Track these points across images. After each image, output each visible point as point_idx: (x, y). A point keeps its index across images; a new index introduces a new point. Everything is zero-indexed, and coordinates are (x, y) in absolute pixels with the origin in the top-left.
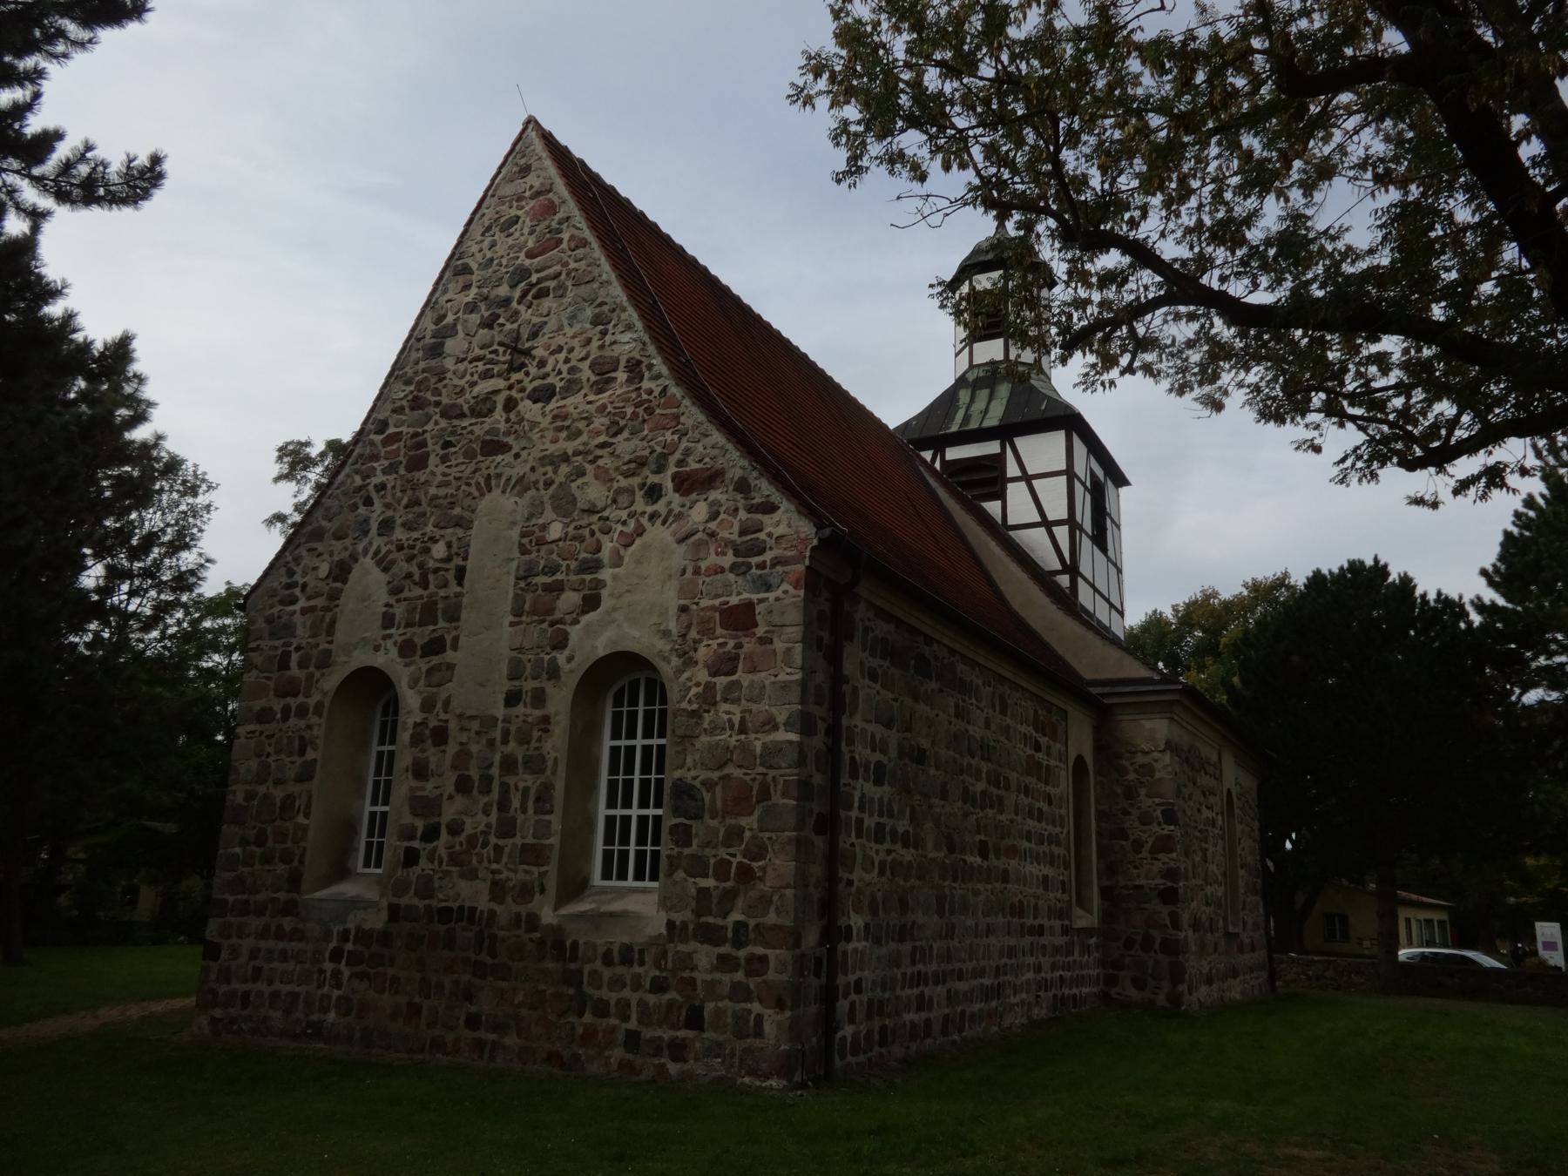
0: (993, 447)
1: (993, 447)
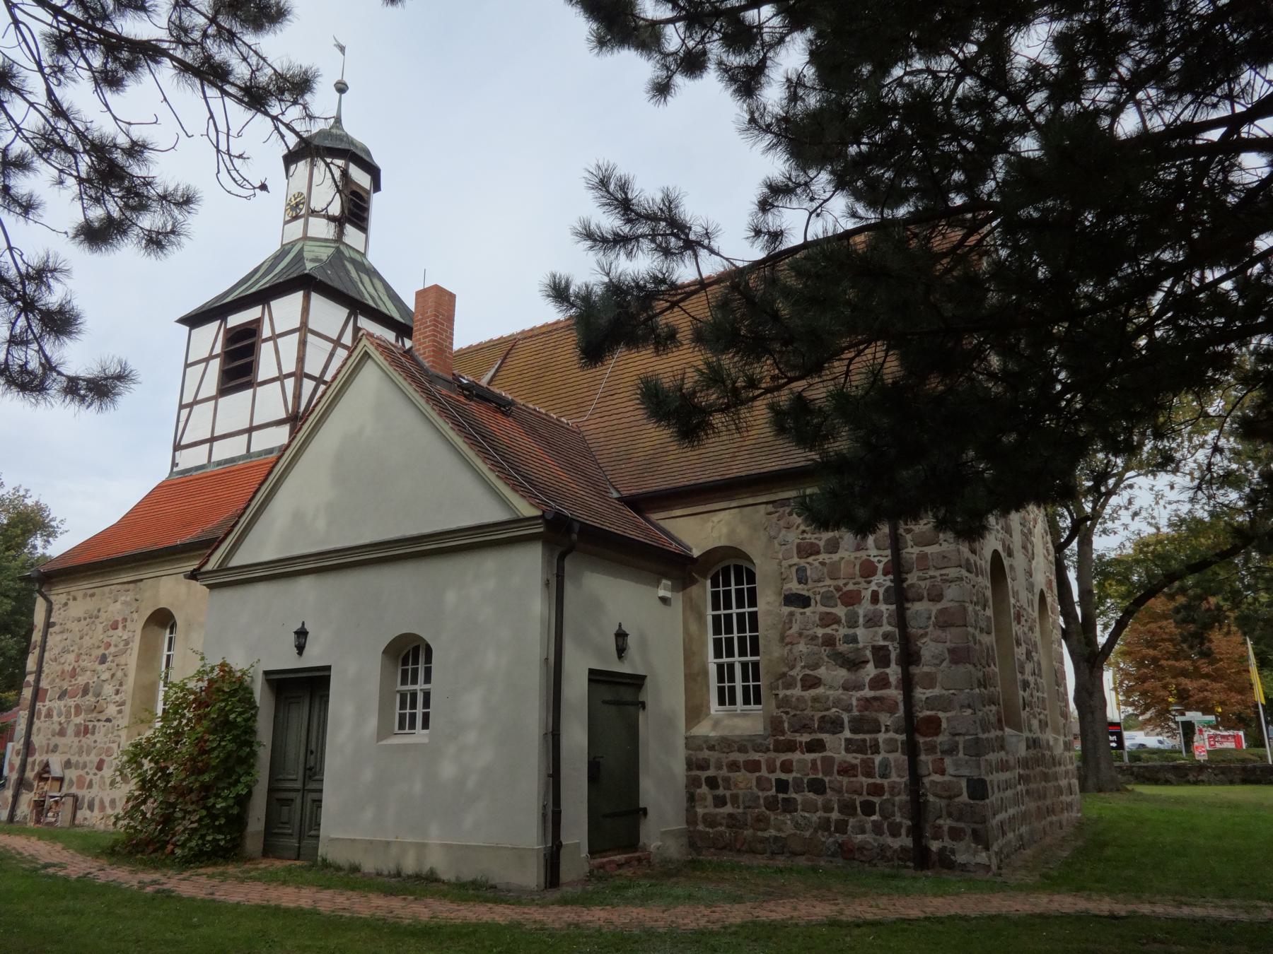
0: (253, 313)
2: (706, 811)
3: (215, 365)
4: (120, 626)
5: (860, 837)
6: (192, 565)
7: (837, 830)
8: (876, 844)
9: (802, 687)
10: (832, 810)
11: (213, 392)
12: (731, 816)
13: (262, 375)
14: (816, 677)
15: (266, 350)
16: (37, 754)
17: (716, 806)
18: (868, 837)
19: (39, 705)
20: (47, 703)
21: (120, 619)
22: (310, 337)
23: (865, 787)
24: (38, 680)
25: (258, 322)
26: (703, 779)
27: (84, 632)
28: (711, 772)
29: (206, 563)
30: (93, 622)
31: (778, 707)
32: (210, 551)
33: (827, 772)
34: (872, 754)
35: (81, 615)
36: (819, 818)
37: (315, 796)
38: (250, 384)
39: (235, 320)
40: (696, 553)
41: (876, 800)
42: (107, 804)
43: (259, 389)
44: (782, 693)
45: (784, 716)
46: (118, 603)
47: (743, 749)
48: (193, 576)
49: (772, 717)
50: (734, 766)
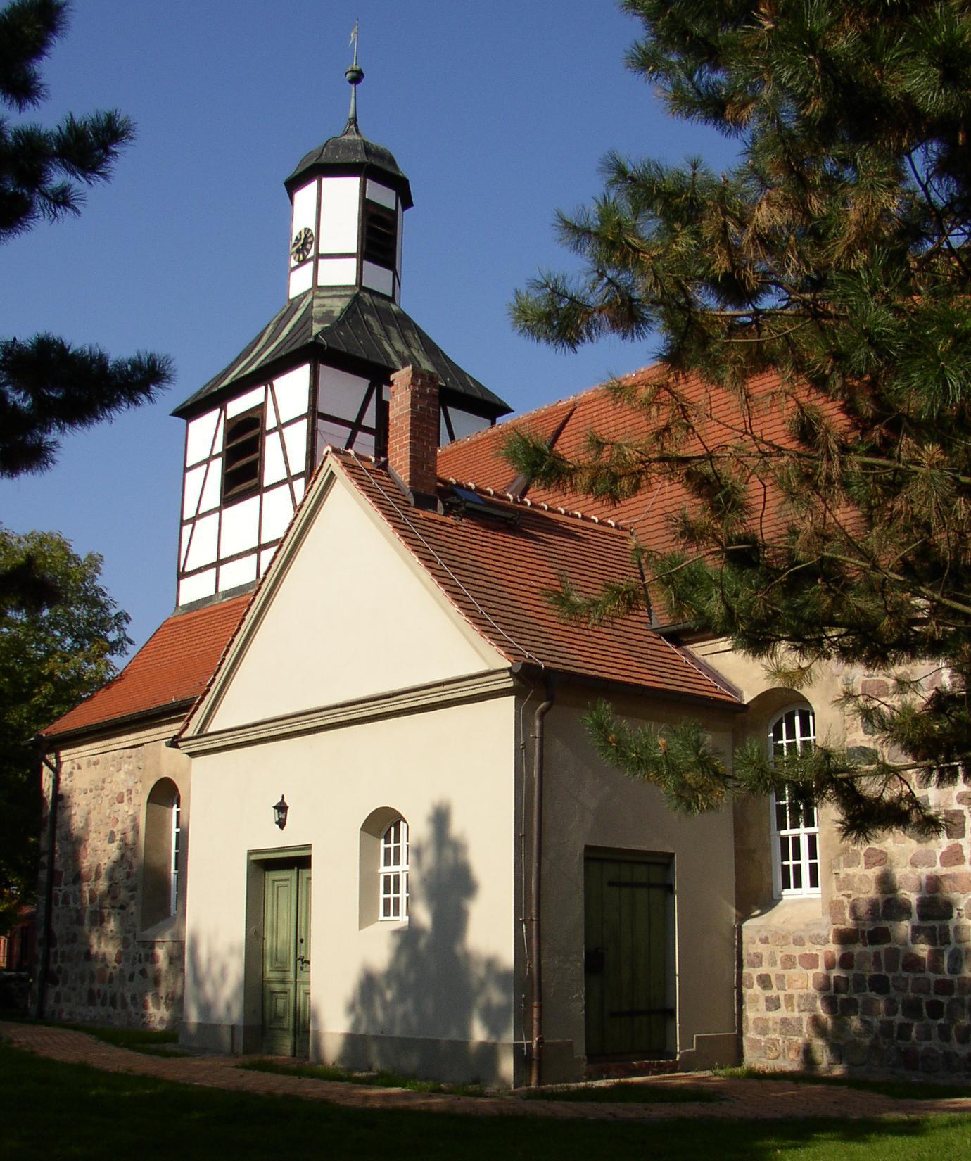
0: (252, 399)
2: (758, 1015)
3: (217, 465)
4: (126, 798)
5: (925, 1044)
6: (171, 730)
7: (899, 1037)
8: (941, 1052)
9: (866, 864)
10: (895, 1012)
11: (217, 503)
12: (784, 1021)
13: (270, 477)
14: (881, 852)
15: (271, 442)
16: (58, 946)
17: (768, 1009)
18: (935, 1043)
19: (56, 889)
20: (63, 887)
21: (124, 791)
22: (321, 424)
23: (932, 984)
24: (52, 861)
25: (262, 407)
26: (755, 977)
27: (92, 806)
28: (763, 970)
29: (186, 728)
30: (99, 795)
31: (839, 889)
32: (189, 714)
33: (892, 967)
34: (942, 944)
35: (87, 786)
36: (881, 1022)
37: (305, 987)
38: (259, 490)
39: (238, 407)
40: (747, 698)
41: (943, 999)
42: (129, 1000)
43: (265, 495)
44: (844, 871)
45: (846, 900)
46: (122, 772)
47: (799, 941)
48: (174, 743)
49: (832, 902)
50: (789, 962)
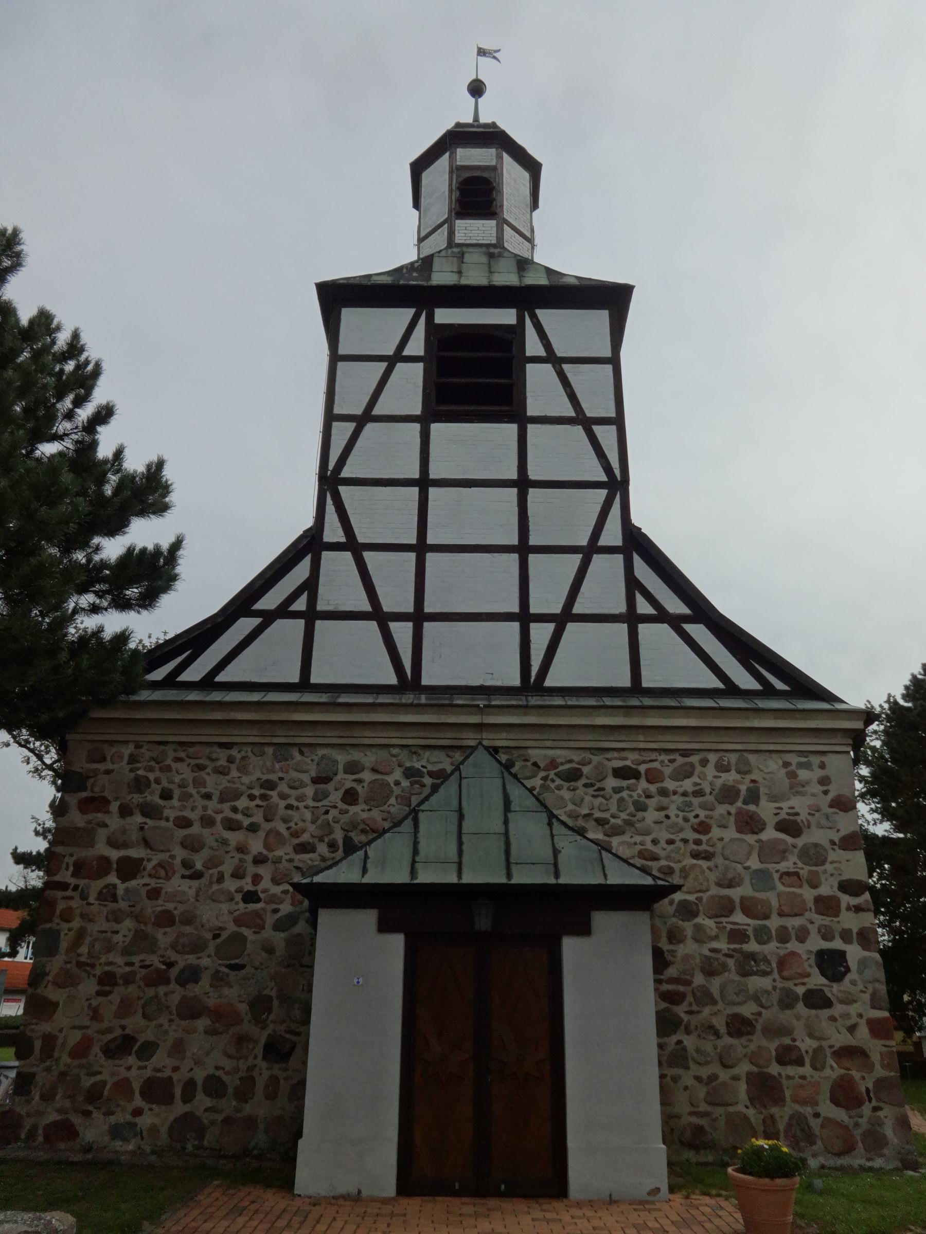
0: (506, 317)
1: (506, 317)
